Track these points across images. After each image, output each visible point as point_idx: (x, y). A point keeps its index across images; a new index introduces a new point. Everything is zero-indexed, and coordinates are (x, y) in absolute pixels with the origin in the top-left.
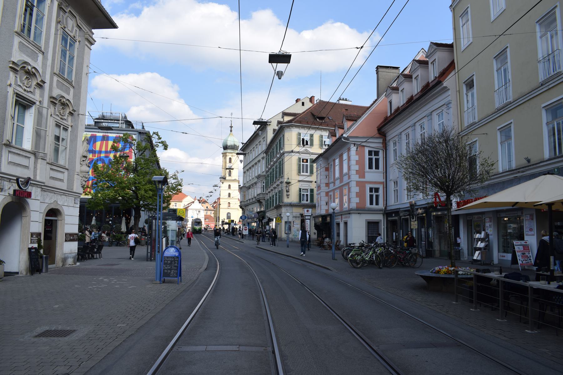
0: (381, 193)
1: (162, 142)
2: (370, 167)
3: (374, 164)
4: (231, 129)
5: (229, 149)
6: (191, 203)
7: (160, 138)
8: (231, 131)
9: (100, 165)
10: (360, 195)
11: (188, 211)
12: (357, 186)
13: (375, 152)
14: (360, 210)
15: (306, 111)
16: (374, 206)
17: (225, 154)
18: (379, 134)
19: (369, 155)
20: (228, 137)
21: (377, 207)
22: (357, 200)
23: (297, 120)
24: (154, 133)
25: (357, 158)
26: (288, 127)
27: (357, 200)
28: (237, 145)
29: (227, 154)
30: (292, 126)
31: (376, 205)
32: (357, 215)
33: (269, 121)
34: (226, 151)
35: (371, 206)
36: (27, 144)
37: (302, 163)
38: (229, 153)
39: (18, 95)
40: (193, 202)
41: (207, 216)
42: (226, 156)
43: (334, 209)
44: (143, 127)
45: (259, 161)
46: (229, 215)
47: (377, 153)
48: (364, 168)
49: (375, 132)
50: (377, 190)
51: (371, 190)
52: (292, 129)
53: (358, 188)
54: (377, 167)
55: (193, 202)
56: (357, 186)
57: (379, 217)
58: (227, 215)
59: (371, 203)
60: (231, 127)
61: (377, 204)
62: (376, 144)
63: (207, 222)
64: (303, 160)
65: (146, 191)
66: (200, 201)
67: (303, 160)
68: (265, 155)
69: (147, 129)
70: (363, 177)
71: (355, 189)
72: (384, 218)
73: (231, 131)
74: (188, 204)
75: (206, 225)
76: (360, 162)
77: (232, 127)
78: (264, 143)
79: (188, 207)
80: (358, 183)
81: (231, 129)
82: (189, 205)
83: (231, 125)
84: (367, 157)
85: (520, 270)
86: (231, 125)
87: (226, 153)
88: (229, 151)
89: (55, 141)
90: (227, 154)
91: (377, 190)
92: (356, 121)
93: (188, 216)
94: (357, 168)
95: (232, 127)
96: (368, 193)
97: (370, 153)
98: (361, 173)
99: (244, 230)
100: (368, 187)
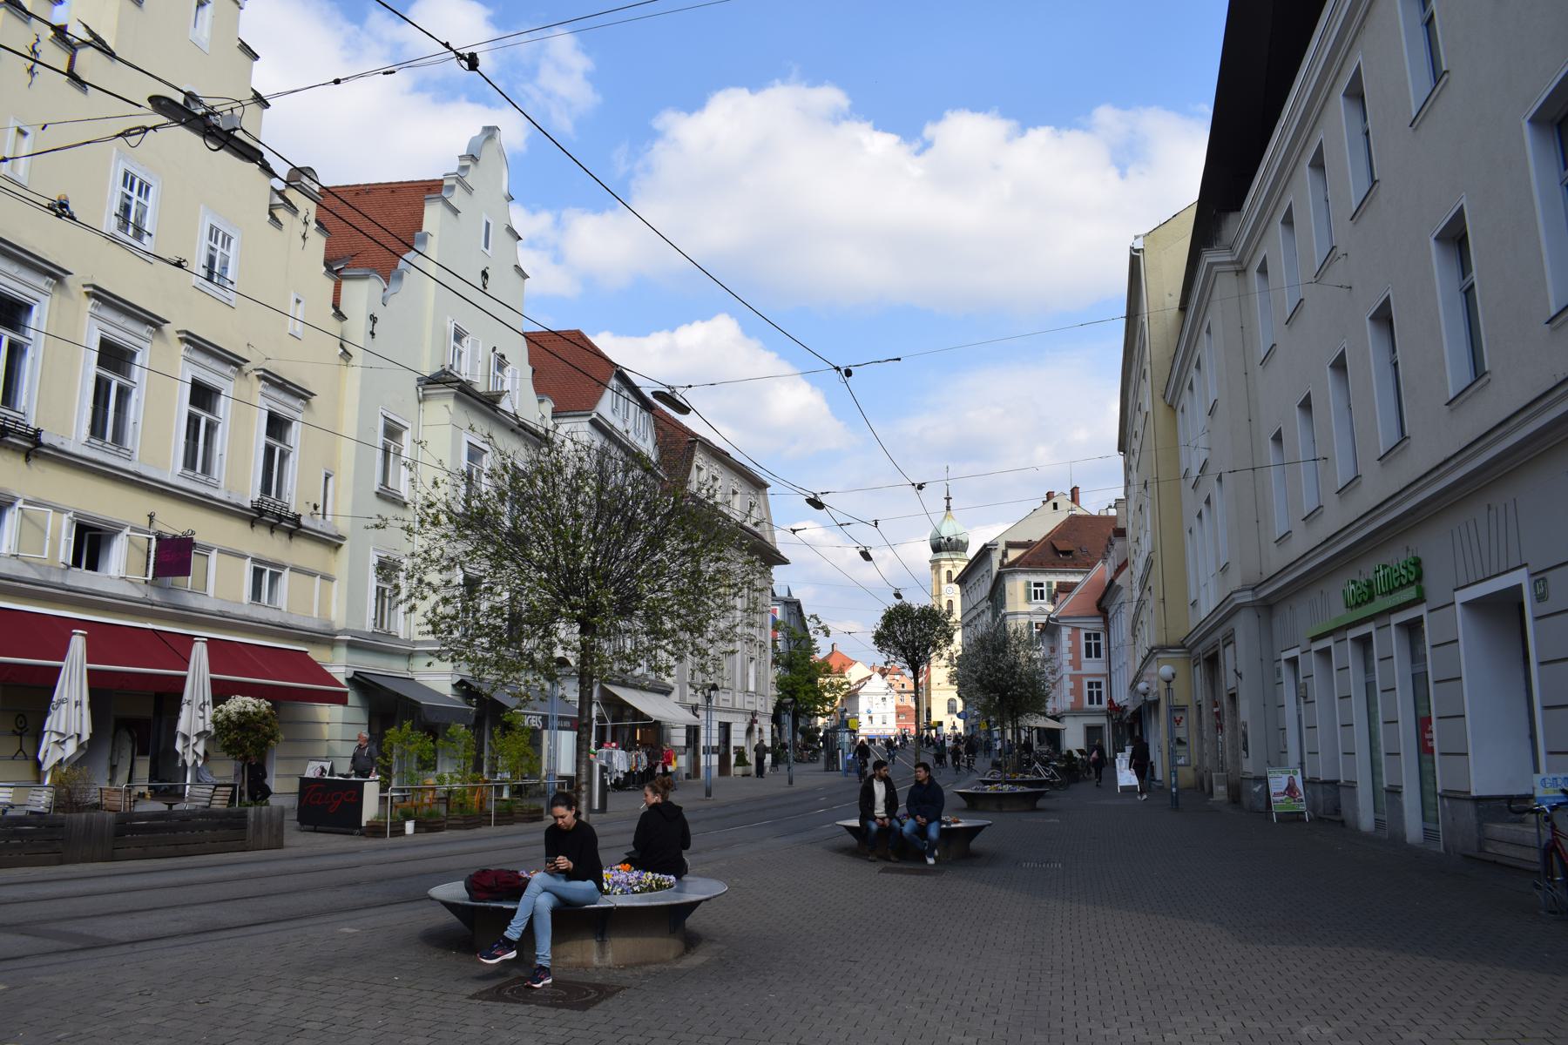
0: (1104, 688)
1: (822, 628)
2: (1089, 655)
3: (1093, 651)
4: (948, 503)
5: (944, 551)
6: (865, 678)
7: (820, 623)
8: (948, 508)
9: (704, 629)
10: (1076, 692)
11: (860, 699)
12: (1071, 680)
13: (1095, 635)
14: (1076, 711)
15: (1044, 538)
16: (1095, 706)
17: (936, 564)
18: (1099, 610)
19: (1086, 639)
20: (943, 522)
21: (1098, 706)
22: (1072, 699)
23: (1026, 561)
24: (812, 616)
25: (1070, 644)
26: (1010, 573)
27: (1072, 699)
28: (964, 541)
29: (942, 562)
30: (1016, 572)
31: (1098, 704)
32: (1072, 719)
33: (994, 542)
34: (938, 556)
35: (1092, 706)
36: (752, 688)
37: (1035, 630)
38: (946, 560)
39: (469, 443)
40: (869, 678)
41: (901, 710)
42: (940, 567)
43: (1145, 695)
44: (790, 594)
45: (983, 612)
46: (951, 703)
47: (1097, 636)
48: (1080, 657)
49: (1095, 611)
50: (1099, 685)
51: (1090, 685)
52: (1017, 576)
53: (1072, 683)
54: (1098, 655)
55: (869, 678)
56: (1071, 680)
57: (1102, 720)
58: (949, 704)
59: (1091, 702)
60: (948, 499)
61: (1099, 702)
62: (1095, 625)
63: (902, 721)
64: (1037, 624)
65: (806, 693)
66: (887, 671)
67: (1037, 624)
68: (989, 603)
69: (795, 596)
70: (1080, 669)
71: (1068, 685)
72: (1108, 721)
73: (948, 508)
74: (859, 682)
75: (901, 730)
76: (1074, 650)
77: (951, 498)
78: (989, 580)
79: (859, 689)
80: (1072, 677)
81: (948, 503)
82: (862, 684)
83: (948, 495)
84: (1083, 641)
85: (1548, 811)
86: (948, 495)
87: (939, 560)
88: (945, 555)
89: (385, 437)
90: (942, 562)
91: (1099, 685)
92: (1070, 592)
93: (860, 710)
94: (1070, 657)
95: (951, 498)
96: (1086, 690)
97: (1088, 636)
98: (1076, 664)
99: (946, 740)
100: (1085, 681)
